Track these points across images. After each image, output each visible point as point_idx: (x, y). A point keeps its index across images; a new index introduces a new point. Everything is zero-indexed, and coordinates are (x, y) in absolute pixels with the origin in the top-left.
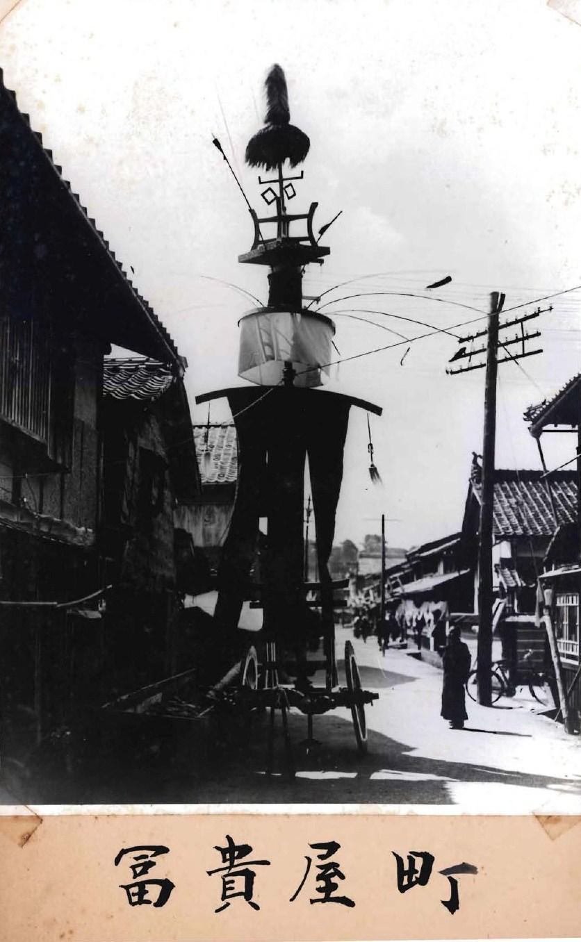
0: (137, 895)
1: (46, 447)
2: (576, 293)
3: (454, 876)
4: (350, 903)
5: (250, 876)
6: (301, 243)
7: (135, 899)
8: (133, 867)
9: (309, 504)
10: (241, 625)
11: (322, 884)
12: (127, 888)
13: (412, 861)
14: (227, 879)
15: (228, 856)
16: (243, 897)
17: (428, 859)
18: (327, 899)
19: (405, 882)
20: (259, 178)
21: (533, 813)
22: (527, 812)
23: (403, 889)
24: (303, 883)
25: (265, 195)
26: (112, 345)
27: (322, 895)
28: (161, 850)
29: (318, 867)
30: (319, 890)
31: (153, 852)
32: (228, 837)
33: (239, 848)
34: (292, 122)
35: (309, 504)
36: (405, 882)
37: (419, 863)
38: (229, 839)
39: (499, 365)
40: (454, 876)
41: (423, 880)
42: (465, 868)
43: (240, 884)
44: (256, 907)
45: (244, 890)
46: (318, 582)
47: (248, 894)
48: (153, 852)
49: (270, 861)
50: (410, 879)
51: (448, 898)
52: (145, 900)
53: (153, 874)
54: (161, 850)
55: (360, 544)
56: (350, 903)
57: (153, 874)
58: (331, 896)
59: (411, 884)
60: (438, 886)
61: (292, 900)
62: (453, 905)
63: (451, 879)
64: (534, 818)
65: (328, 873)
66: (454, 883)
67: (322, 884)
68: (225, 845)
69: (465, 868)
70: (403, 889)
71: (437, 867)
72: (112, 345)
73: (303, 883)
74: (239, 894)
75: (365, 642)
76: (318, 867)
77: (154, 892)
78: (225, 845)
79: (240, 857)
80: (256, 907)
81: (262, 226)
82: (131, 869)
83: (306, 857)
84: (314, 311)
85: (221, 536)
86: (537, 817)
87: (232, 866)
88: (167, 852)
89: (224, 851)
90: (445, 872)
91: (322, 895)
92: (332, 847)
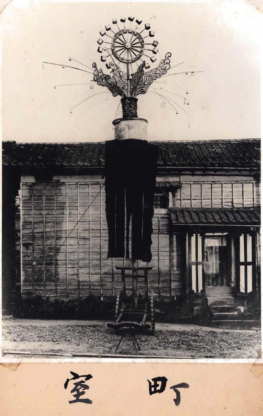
3: (178, 389)
9: (162, 99)
17: (164, 380)
18: (78, 400)
19: (153, 389)
20: (71, 402)
23: (151, 393)
27: (75, 398)
30: (75, 396)
32: (170, 388)
34: (252, 291)
35: (162, 99)
37: (159, 383)
40: (178, 389)
42: (184, 385)
46: (157, 185)
50: (155, 389)
55: (169, 180)
56: (88, 401)
59: (156, 391)
60: (169, 394)
62: (177, 401)
66: (178, 394)
67: (75, 393)
69: (184, 385)
70: (151, 393)
71: (169, 385)
81: (232, 191)
84: (240, 284)
88: (85, 393)
90: (174, 388)
91: (75, 398)
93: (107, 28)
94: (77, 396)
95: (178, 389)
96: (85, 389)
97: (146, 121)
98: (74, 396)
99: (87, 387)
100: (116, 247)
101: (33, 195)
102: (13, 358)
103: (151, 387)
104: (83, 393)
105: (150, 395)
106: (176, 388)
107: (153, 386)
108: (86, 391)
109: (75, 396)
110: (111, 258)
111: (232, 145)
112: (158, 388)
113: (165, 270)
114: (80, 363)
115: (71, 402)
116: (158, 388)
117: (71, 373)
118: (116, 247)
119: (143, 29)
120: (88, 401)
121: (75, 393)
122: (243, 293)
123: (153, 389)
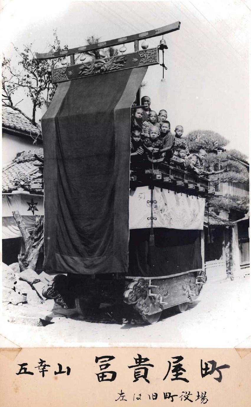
0: (101, 377)
1: (43, 198)
5: (146, 370)
6: (133, 125)
7: (101, 379)
8: (100, 366)
12: (98, 375)
14: (136, 371)
15: (138, 361)
16: (142, 378)
18: (177, 379)
21: (235, 347)
22: (233, 347)
23: (203, 376)
27: (175, 377)
28: (111, 358)
29: (173, 366)
31: (108, 359)
32: (215, 378)
38: (41, 360)
39: (186, 195)
40: (220, 370)
42: (226, 366)
43: (142, 372)
44: (148, 381)
45: (143, 375)
47: (145, 376)
48: (108, 359)
49: (57, 364)
50: (206, 372)
52: (27, 372)
53: (109, 369)
54: (111, 358)
56: (187, 381)
57: (109, 369)
59: (207, 374)
61: (164, 379)
64: (235, 350)
67: (175, 373)
68: (137, 357)
70: (203, 376)
74: (142, 376)
76: (173, 366)
77: (109, 376)
78: (137, 357)
79: (144, 362)
80: (148, 381)
83: (59, 364)
86: (236, 349)
87: (140, 365)
89: (136, 360)
91: (175, 377)
92: (180, 358)
93: (58, 371)
94: (177, 375)
95: (220, 370)
98: (174, 375)
101: (225, 169)
103: (202, 369)
104: (181, 374)
105: (115, 358)
106: (219, 370)
107: (204, 369)
110: (154, 226)
114: (81, 347)
119: (8, 229)
120: (185, 380)
121: (175, 373)
122: (61, 370)
123: (204, 372)
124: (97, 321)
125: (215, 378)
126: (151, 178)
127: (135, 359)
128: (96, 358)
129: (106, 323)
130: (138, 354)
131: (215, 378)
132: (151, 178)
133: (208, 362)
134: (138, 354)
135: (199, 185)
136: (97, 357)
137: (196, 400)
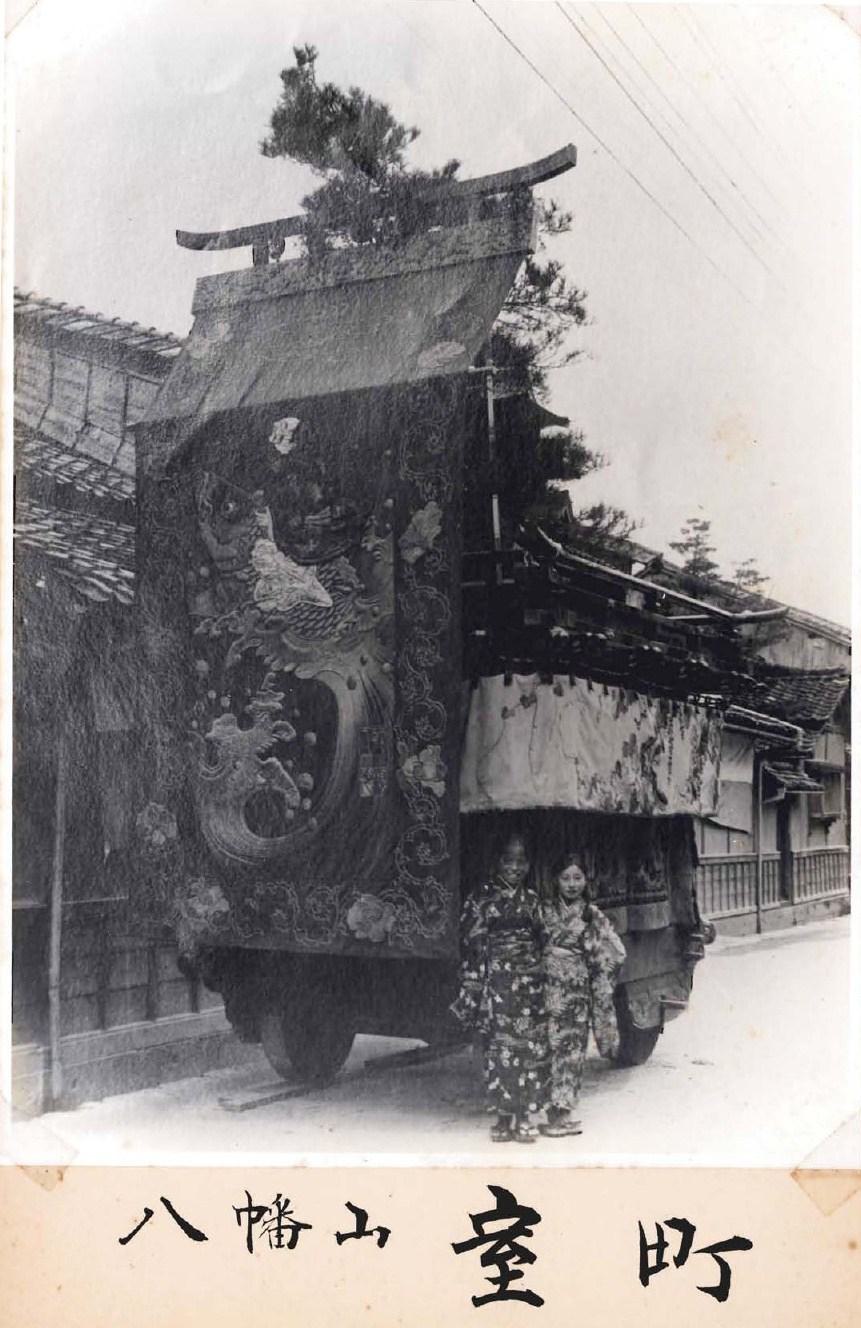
2: (576, 787)
3: (720, 1254)
4: (534, 1300)
10: (499, 1275)
11: (494, 1271)
13: (660, 1232)
17: (686, 1228)
18: (503, 1295)
19: (652, 1262)
20: (478, 1302)
23: (645, 1274)
24: (135, 1232)
25: (242, 1214)
26: (514, 1240)
27: (495, 1289)
30: (494, 1281)
33: (256, 1209)
36: (652, 1262)
37: (674, 1237)
40: (726, 1256)
41: (680, 1260)
51: (715, 1281)
56: (534, 1300)
58: (509, 1288)
59: (661, 1265)
62: (721, 1292)
63: (720, 1260)
65: (500, 1252)
71: (700, 1240)
72: (514, 1240)
73: (135, 1232)
75: (616, 717)
82: (344, 1243)
85: (44, 522)
88: (521, 1277)
91: (495, 1289)
96: (525, 1262)
97: (123, 1241)
99: (528, 1257)
100: (619, 674)
102: (794, 609)
103: (644, 1248)
104: (519, 1274)
105: (453, 1245)
108: (524, 1267)
109: (494, 1281)
111: (544, 811)
112: (670, 1254)
113: (330, 1099)
115: (478, 1302)
116: (670, 1254)
117: (531, 1211)
118: (619, 674)
124: (19, 657)
125: (699, 1288)
126: (482, 633)
127: (470, 1216)
128: (473, 1221)
129: (263, 225)
130: (491, 1188)
131: (699, 1288)
132: (482, 633)
133: (667, 1223)
134: (491, 1188)
135: (699, 627)
136: (667, 1268)
137: (197, 1236)
